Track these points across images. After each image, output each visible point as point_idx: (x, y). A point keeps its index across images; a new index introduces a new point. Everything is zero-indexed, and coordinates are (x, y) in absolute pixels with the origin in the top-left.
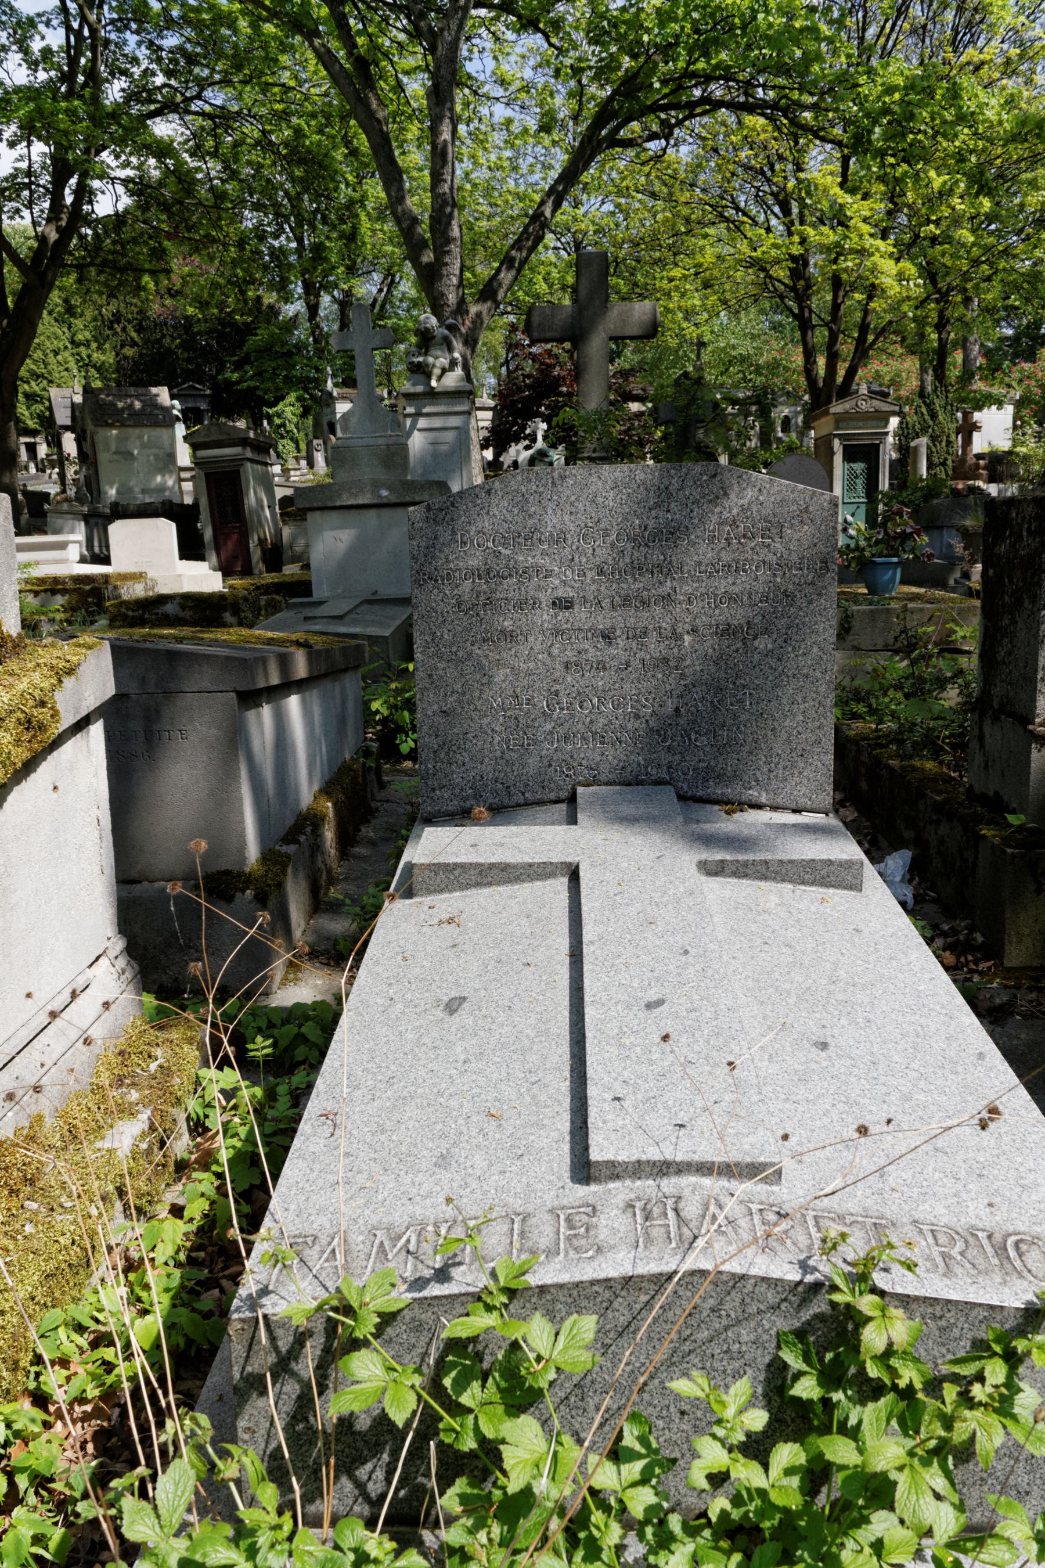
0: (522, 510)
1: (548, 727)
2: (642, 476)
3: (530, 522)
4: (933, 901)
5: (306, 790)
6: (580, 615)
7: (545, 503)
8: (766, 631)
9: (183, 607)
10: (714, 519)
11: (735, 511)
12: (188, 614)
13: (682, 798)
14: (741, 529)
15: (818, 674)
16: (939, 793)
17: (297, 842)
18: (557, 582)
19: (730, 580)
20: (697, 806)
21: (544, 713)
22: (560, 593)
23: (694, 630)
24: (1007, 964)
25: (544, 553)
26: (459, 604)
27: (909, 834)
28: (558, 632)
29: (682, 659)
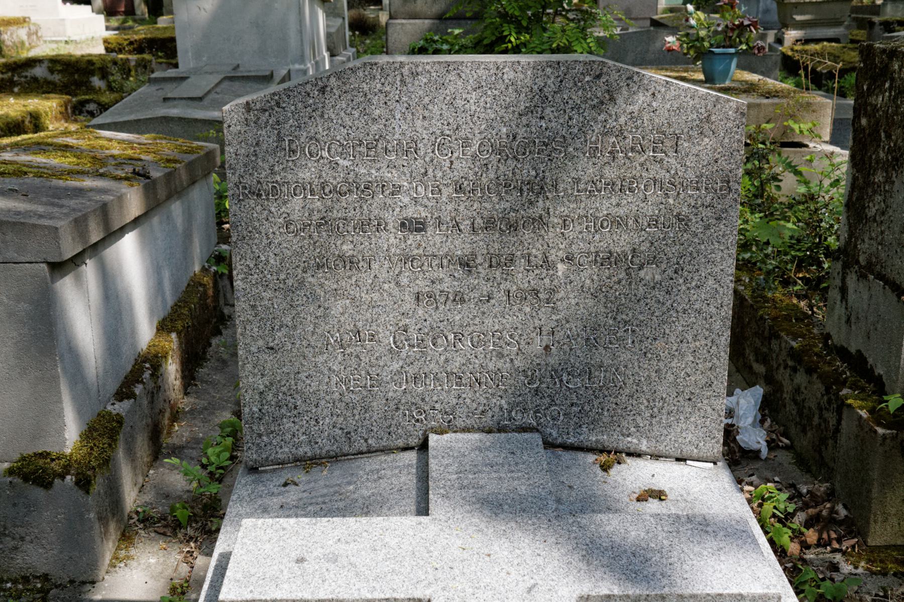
0: (364, 113)
1: (396, 366)
2: (512, 75)
3: (374, 128)
4: (786, 448)
5: (145, 332)
6: (434, 239)
7: (392, 104)
8: (654, 260)
9: (51, 71)
10: (597, 128)
11: (622, 120)
12: (56, 78)
13: (549, 445)
14: (629, 141)
15: (713, 309)
16: (795, 337)
17: (131, 395)
18: (406, 200)
19: (614, 201)
20: (566, 456)
21: (390, 351)
22: (410, 212)
23: (569, 258)
24: (871, 542)
25: (391, 166)
26: (288, 224)
27: (760, 368)
28: (407, 259)
29: (553, 291)
